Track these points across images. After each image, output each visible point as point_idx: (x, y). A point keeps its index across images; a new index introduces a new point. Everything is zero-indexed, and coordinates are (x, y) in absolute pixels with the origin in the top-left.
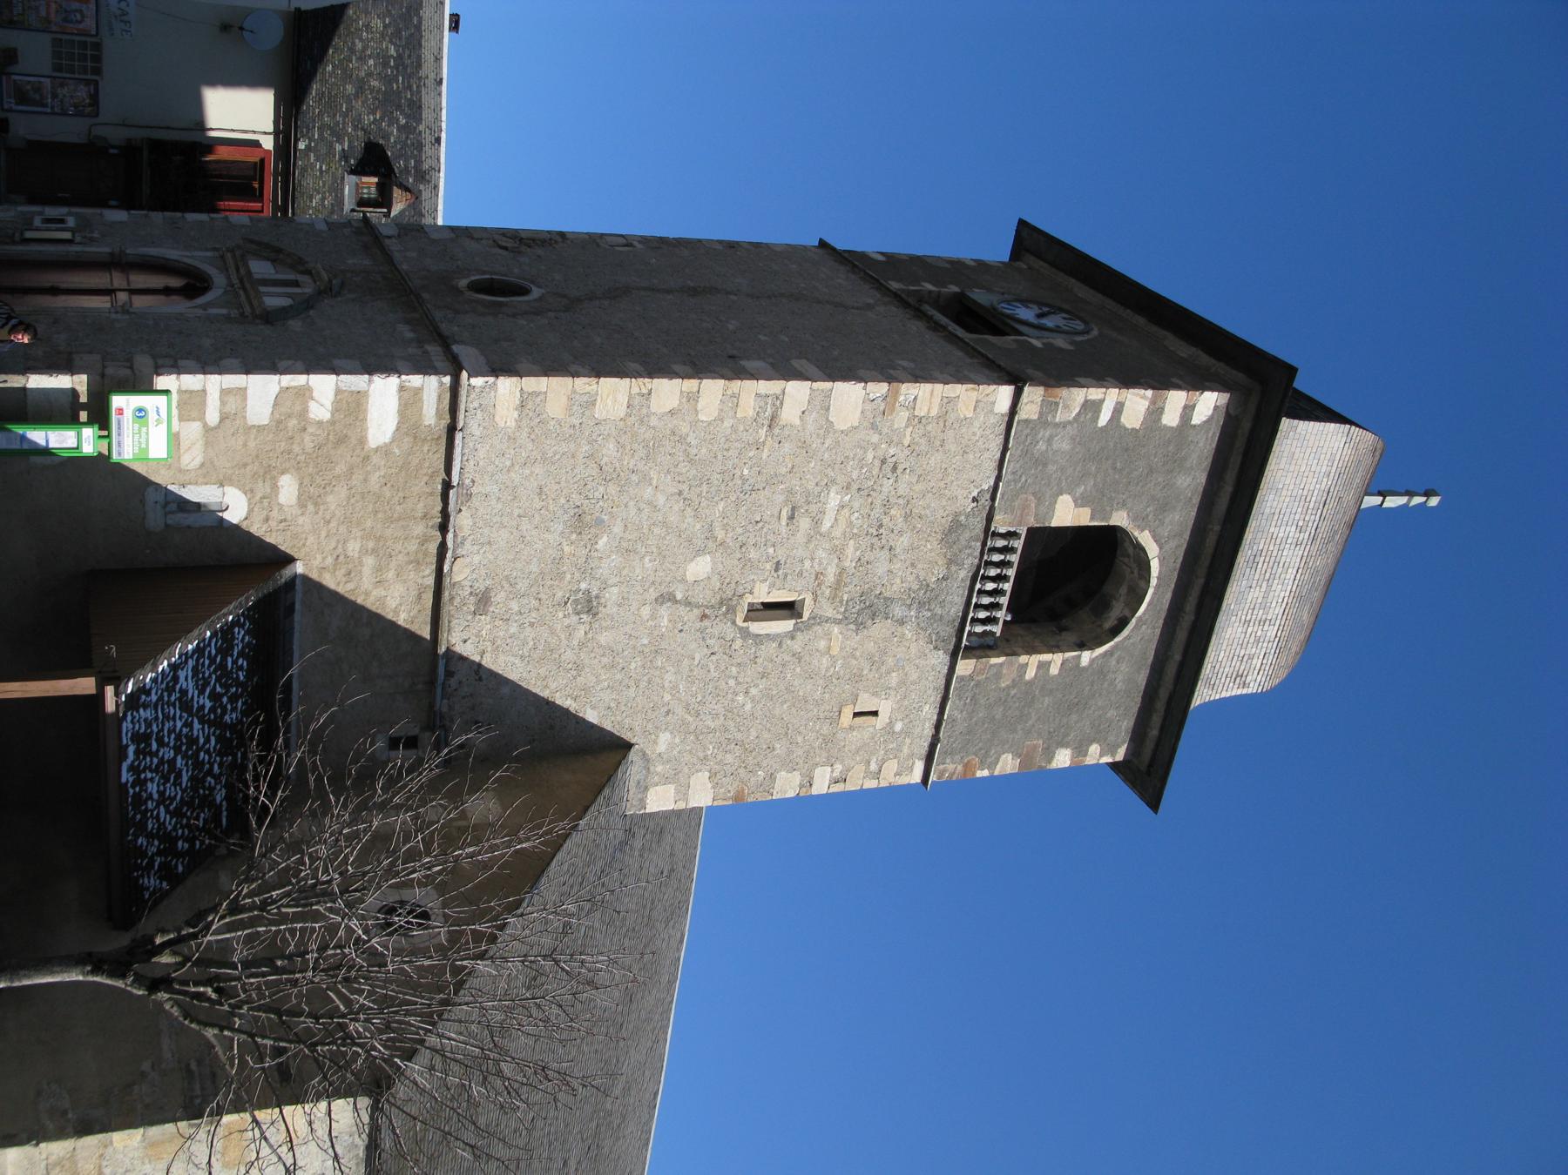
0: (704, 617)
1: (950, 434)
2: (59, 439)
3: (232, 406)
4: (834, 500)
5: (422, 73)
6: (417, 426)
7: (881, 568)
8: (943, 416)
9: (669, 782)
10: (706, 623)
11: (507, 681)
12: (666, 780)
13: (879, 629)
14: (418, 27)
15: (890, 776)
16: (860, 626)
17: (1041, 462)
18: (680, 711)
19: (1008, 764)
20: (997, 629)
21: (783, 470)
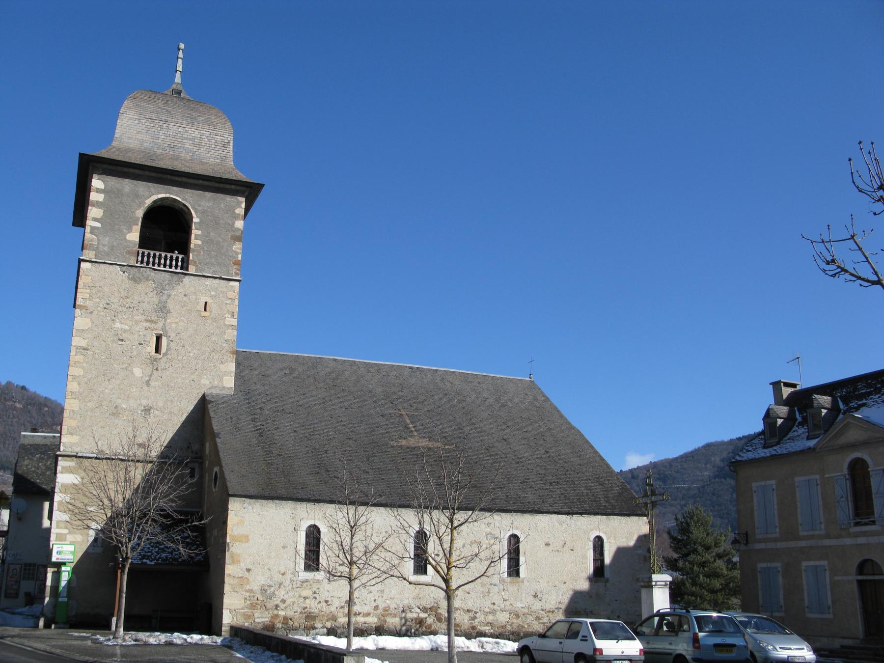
0: (157, 369)
1: (97, 285)
2: (65, 577)
3: (63, 525)
4: (118, 325)
5: (49, 443)
6: (74, 468)
7: (145, 306)
8: (90, 288)
9: (223, 379)
10: (159, 368)
11: (173, 438)
12: (221, 380)
13: (170, 305)
14: (31, 445)
15: (235, 295)
16: (169, 312)
17: (112, 248)
18: (193, 377)
19: (237, 247)
20: (181, 257)
21: (104, 344)
